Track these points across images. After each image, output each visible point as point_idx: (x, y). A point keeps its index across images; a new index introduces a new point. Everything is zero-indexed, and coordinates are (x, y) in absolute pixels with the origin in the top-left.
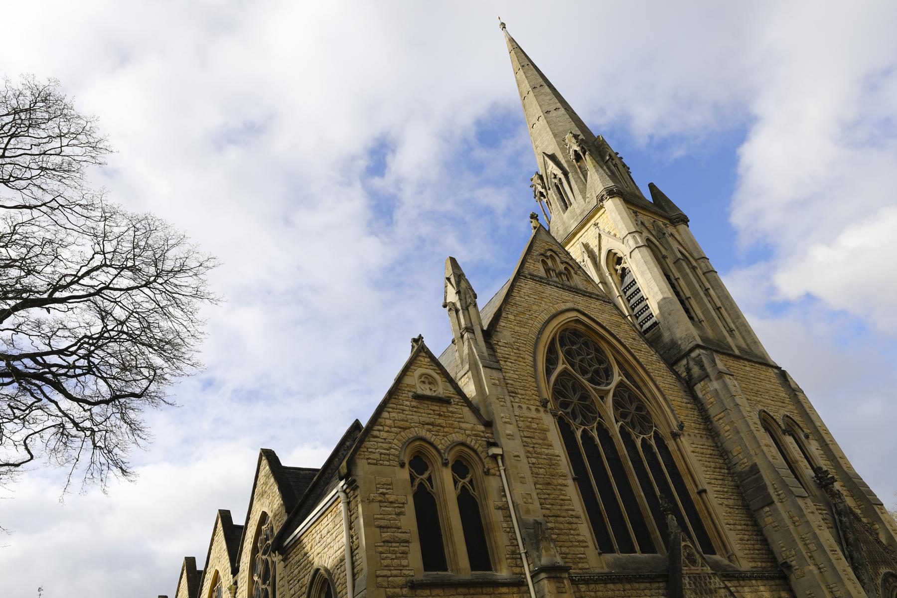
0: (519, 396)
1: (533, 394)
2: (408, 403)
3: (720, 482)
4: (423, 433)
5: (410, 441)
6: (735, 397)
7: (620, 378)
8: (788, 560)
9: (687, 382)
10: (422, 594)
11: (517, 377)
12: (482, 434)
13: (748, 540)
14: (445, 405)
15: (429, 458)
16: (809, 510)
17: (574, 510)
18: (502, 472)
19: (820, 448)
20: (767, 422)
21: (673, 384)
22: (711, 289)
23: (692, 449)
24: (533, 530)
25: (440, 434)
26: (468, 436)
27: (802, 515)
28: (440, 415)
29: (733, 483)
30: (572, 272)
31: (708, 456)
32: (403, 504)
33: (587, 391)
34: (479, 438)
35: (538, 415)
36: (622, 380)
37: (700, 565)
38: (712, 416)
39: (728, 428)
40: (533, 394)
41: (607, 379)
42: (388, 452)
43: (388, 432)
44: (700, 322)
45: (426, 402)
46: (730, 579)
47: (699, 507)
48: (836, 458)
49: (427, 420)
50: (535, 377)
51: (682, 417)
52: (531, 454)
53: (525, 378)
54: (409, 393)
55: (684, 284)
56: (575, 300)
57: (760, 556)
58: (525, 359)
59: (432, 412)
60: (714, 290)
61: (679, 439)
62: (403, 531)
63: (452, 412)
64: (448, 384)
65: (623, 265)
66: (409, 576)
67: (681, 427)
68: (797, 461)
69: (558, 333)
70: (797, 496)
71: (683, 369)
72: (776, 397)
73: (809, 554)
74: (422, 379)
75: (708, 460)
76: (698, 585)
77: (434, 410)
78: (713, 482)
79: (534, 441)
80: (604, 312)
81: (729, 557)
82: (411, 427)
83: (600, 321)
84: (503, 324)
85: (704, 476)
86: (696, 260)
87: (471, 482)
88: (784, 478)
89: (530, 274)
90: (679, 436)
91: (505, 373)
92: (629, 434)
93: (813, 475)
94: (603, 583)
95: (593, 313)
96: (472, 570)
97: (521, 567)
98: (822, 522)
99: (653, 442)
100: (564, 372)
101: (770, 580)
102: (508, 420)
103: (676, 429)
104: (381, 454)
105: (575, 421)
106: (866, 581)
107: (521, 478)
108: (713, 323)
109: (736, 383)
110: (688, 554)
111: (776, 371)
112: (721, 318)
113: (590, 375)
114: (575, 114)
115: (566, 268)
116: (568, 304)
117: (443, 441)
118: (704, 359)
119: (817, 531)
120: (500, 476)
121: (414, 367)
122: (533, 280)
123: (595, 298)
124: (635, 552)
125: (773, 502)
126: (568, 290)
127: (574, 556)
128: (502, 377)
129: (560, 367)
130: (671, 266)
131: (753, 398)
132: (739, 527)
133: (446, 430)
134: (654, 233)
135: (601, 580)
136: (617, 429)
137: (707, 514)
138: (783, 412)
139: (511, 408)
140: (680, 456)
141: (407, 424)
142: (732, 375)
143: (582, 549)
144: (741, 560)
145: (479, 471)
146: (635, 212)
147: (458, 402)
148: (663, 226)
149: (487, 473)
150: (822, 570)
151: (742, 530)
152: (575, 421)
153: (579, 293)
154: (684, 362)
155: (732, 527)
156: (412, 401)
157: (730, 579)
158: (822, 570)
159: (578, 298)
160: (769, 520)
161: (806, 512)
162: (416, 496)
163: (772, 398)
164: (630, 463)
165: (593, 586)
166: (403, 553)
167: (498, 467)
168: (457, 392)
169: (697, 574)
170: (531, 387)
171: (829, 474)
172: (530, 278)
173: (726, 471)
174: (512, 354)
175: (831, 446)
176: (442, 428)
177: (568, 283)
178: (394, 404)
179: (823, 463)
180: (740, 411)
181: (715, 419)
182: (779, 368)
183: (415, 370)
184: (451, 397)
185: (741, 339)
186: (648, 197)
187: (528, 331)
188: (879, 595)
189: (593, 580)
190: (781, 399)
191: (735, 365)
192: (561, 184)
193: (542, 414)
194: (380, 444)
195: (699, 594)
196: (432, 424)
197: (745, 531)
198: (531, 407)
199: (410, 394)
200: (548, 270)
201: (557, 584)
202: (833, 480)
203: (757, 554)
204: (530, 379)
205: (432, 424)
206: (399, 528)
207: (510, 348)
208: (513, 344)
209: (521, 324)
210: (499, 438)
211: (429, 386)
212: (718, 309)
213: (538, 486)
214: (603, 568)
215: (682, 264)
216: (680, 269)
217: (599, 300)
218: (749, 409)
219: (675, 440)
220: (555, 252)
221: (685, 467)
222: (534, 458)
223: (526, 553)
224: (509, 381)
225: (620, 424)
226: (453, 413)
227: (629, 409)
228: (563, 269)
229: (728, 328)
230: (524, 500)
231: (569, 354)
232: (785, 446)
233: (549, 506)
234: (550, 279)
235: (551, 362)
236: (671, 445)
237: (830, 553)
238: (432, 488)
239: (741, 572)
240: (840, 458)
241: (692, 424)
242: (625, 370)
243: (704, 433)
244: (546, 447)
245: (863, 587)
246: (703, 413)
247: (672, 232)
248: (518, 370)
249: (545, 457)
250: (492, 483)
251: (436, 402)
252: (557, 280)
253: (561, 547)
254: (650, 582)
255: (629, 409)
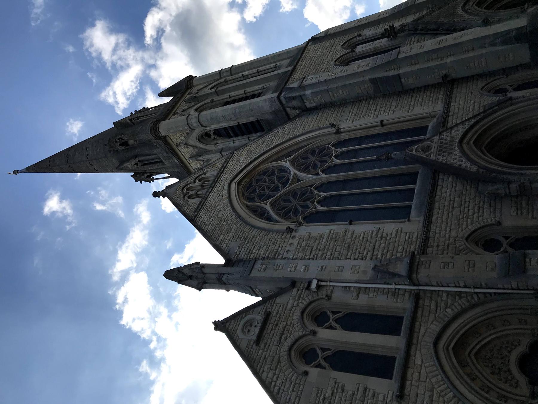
0: (279, 250)
1: (281, 237)
2: (261, 351)
3: (378, 107)
4: (286, 345)
5: (289, 360)
6: (320, 81)
7: (288, 161)
8: (442, 75)
9: (303, 111)
10: (409, 389)
11: (265, 246)
12: (300, 292)
13: (422, 99)
14: (270, 317)
15: (307, 346)
16: (409, 51)
17: (373, 231)
18: (331, 284)
19: (370, 29)
20: (344, 61)
21: (302, 122)
22: (243, 73)
23: (351, 122)
24: (379, 273)
25: (291, 330)
26: (298, 305)
27: (411, 57)
28: (277, 325)
29: (381, 98)
30: (203, 176)
31: (358, 111)
32: (336, 382)
33: (290, 191)
34: (302, 296)
35: (297, 238)
36: (289, 161)
37: (432, 143)
38: (330, 100)
39: (341, 92)
40: (281, 237)
41: (287, 172)
42: (293, 383)
43: (277, 378)
44: (264, 89)
45: (264, 334)
46: (446, 122)
47: (393, 128)
48: (379, 20)
49: (277, 338)
50: (269, 231)
51: (326, 123)
52: (324, 254)
53: (268, 240)
54: (253, 347)
55: (234, 92)
56: (224, 181)
57: (435, 94)
58: (254, 236)
59: (272, 332)
60: (245, 71)
61: (341, 130)
62: (356, 390)
63: (277, 314)
64: (256, 309)
65: (211, 133)
66: (392, 397)
67: (333, 125)
68: (375, 48)
69: (243, 200)
70: (397, 57)
71: (293, 111)
72: (328, 49)
73: (439, 60)
74: (246, 331)
75: (361, 112)
76: (445, 150)
77: (272, 329)
78: (377, 113)
79: (315, 248)
80: (238, 160)
81: (432, 117)
82: (279, 354)
83: (244, 166)
84: (224, 246)
85: (371, 118)
86: (221, 78)
87: (334, 313)
88: (383, 63)
89: (195, 212)
90: (339, 129)
91: (260, 256)
92: (329, 167)
93: (386, 39)
94: (431, 224)
95: (237, 169)
96: (399, 335)
97: (405, 291)
98: (419, 44)
99: (340, 150)
100: (272, 204)
101: (453, 92)
102: (294, 266)
103: (333, 130)
104: (293, 390)
105: (310, 208)
106: (465, 25)
107: (338, 270)
108: (268, 80)
109: (310, 77)
110: (422, 150)
111: (310, 43)
112: (266, 72)
113: (280, 185)
114: (95, 136)
115: (199, 181)
116: (225, 187)
117: (297, 329)
118: (288, 96)
119: (425, 49)
120: (334, 286)
121: (235, 336)
122: (200, 210)
123: (227, 164)
124: (414, 189)
125: (398, 75)
126: (215, 184)
127: (406, 243)
128: (261, 261)
129: (268, 207)
130: (219, 99)
131: (324, 67)
132: (413, 103)
133: (289, 323)
134: (193, 104)
135: (428, 225)
136: (322, 175)
137: (399, 124)
138: (339, 48)
139: (286, 261)
140: (353, 132)
141: (276, 360)
142: (304, 78)
143: (402, 234)
144: (436, 109)
145: (326, 304)
146: (175, 114)
147: (271, 305)
148: (190, 96)
149: (329, 298)
150: (452, 54)
151: (415, 102)
152: (310, 208)
153: (220, 176)
154: (288, 109)
155: (411, 108)
156: (260, 347)
157: (446, 122)
158: (452, 54)
159: (223, 178)
160: (411, 81)
161: (409, 54)
162: (335, 367)
163: (328, 53)
164: (349, 173)
165: (431, 233)
166: (373, 396)
167: (327, 286)
168: (263, 303)
169: (437, 148)
170: (276, 237)
171: (387, 29)
172: (198, 212)
173: (372, 101)
174: (248, 245)
175: (369, 21)
176: (287, 327)
177: (211, 182)
178: (258, 364)
179: (380, 29)
180: (330, 80)
181: (333, 98)
182: (309, 41)
183: (238, 336)
184: (266, 311)
185: (283, 62)
186: (167, 100)
187: (235, 227)
188: (475, 19)
189: (427, 233)
190: (330, 46)
191: (297, 75)
192: (142, 161)
193: (297, 234)
194: (285, 389)
195: (452, 151)
196: (282, 335)
197: (416, 99)
198: (290, 242)
199: (254, 346)
200: (197, 196)
201: (423, 266)
202: (392, 27)
203: (433, 96)
204: (269, 236)
205: (282, 335)
206: (354, 394)
207: (243, 246)
208: (241, 242)
209: (228, 232)
210: (305, 279)
211: (253, 326)
212: (259, 73)
213: (349, 257)
214: (419, 221)
215: (220, 90)
216: (224, 92)
217: (229, 161)
218: (330, 73)
219: (341, 133)
220: (186, 186)
221: (362, 131)
222: (327, 253)
223: (396, 284)
224: (267, 255)
225: (320, 172)
226: (278, 313)
227: (312, 162)
228: (199, 183)
229: (274, 69)
230: (355, 273)
231: (261, 197)
232: (363, 53)
233: (365, 252)
234: (203, 196)
235: (262, 214)
236: (344, 136)
237: (441, 46)
238: (330, 350)
239: (444, 112)
240: (379, 16)
241: (333, 116)
242: (283, 156)
243: (341, 109)
244: (322, 239)
245: (469, 28)
246: (328, 105)
247: (197, 90)
248: (261, 244)
249: (329, 242)
250: (338, 296)
251: (266, 325)
252: (206, 190)
253: (397, 251)
254: (437, 186)
255: (312, 162)
